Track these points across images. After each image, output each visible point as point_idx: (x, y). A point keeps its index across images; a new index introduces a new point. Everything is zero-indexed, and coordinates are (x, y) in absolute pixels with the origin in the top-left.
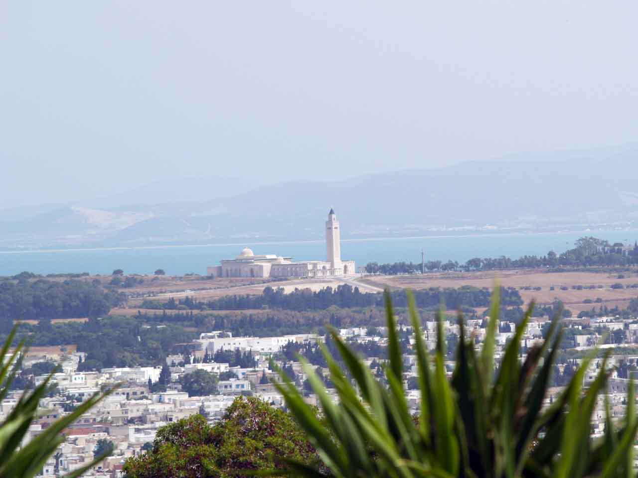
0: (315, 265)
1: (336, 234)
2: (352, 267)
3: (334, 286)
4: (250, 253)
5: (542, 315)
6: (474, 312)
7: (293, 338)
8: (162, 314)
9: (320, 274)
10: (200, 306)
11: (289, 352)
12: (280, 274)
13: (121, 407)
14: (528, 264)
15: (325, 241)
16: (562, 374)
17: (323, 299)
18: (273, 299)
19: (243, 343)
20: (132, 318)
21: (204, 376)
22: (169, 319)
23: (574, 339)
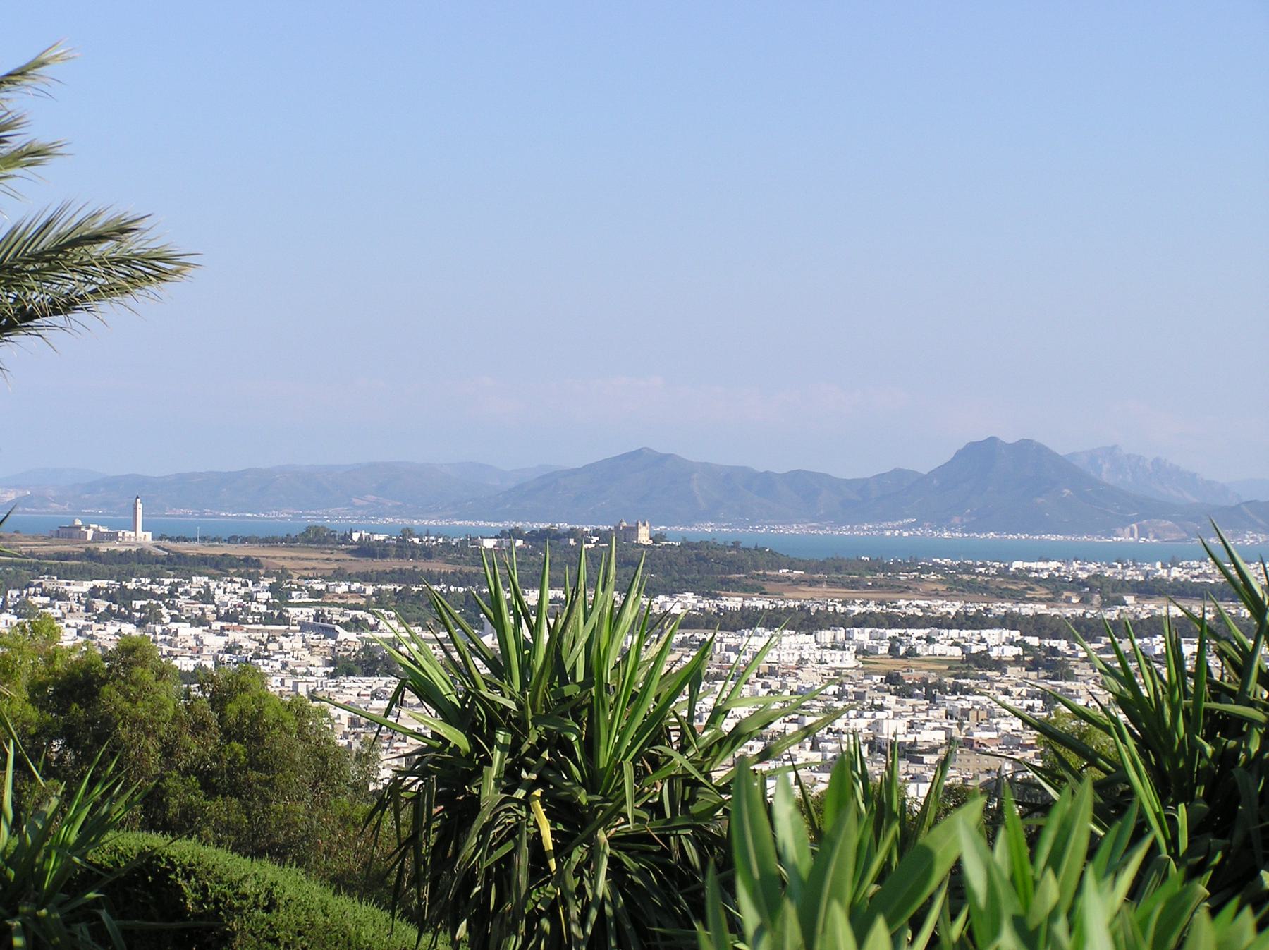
0: (123, 533)
1: (140, 512)
2: (149, 535)
3: (134, 549)
4: (79, 523)
5: (272, 577)
6: (227, 572)
7: (98, 583)
8: (739, 606)
9: (126, 540)
10: (39, 557)
11: (94, 592)
12: (99, 537)
13: (46, 316)
14: (270, 541)
15: (131, 518)
16: (1118, 795)
17: (124, 557)
18: (91, 555)
19: (62, 585)
20: (1074, 935)
21: (57, 624)
22: (16, 565)
23: (291, 594)
